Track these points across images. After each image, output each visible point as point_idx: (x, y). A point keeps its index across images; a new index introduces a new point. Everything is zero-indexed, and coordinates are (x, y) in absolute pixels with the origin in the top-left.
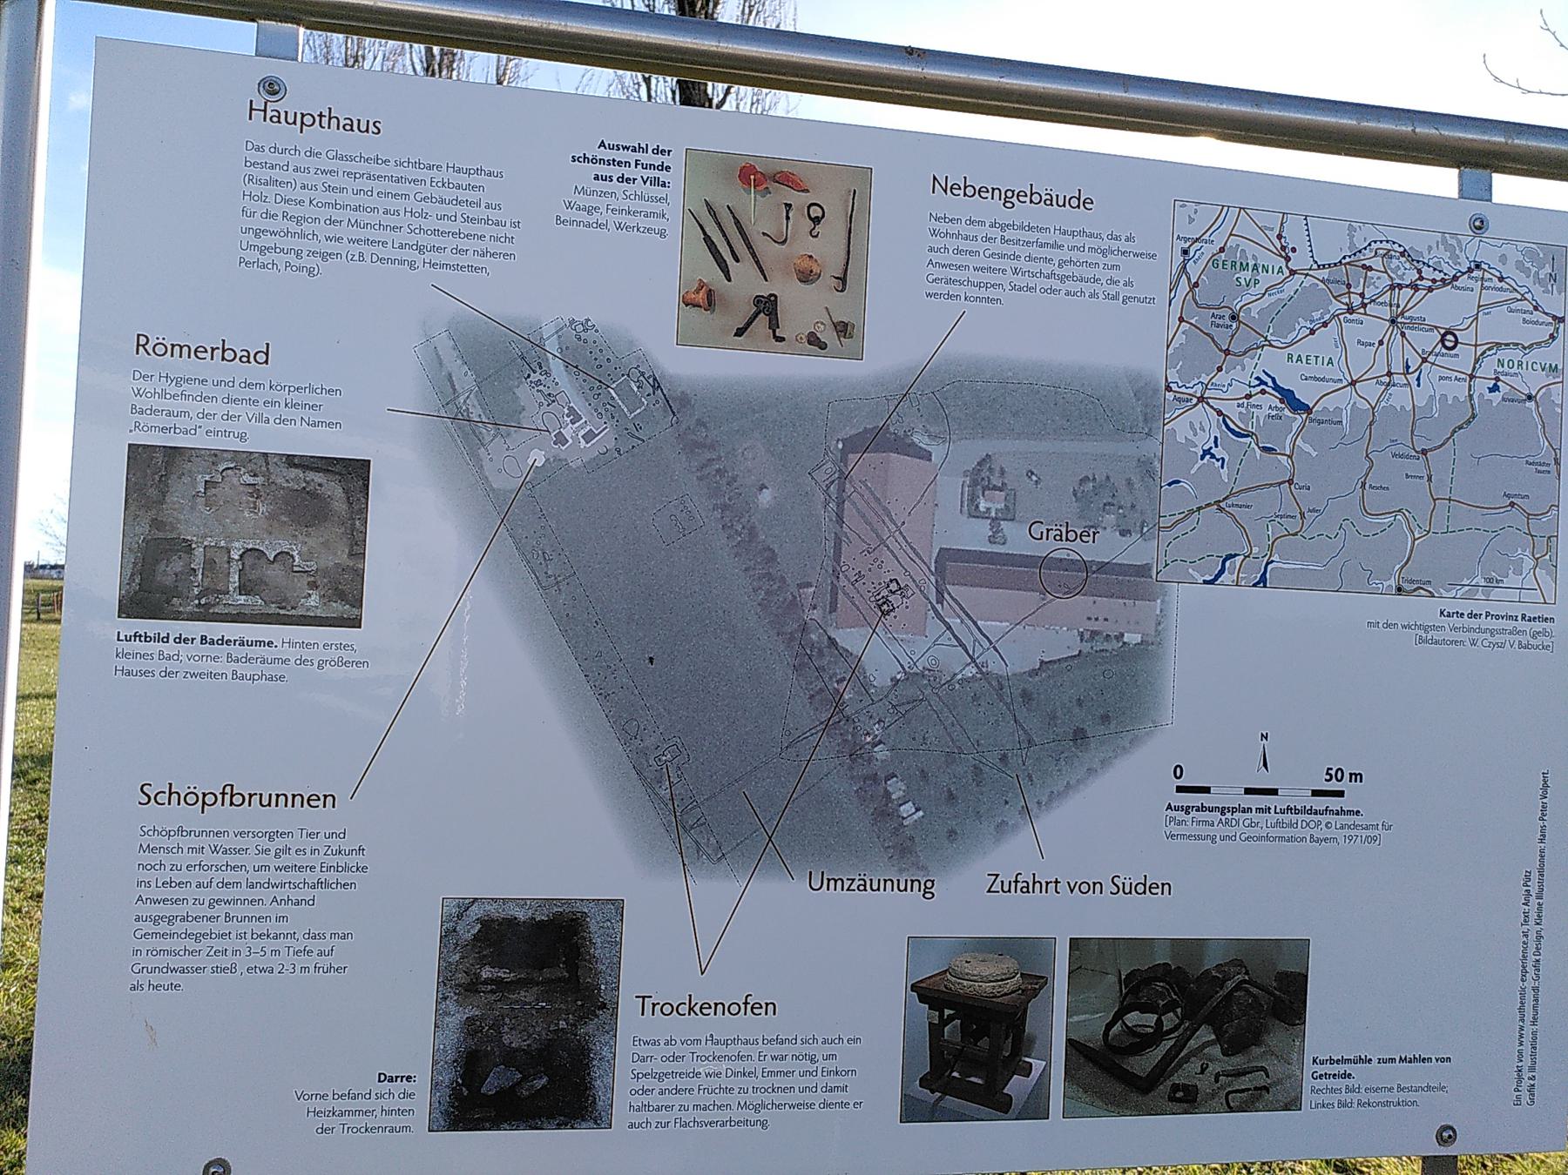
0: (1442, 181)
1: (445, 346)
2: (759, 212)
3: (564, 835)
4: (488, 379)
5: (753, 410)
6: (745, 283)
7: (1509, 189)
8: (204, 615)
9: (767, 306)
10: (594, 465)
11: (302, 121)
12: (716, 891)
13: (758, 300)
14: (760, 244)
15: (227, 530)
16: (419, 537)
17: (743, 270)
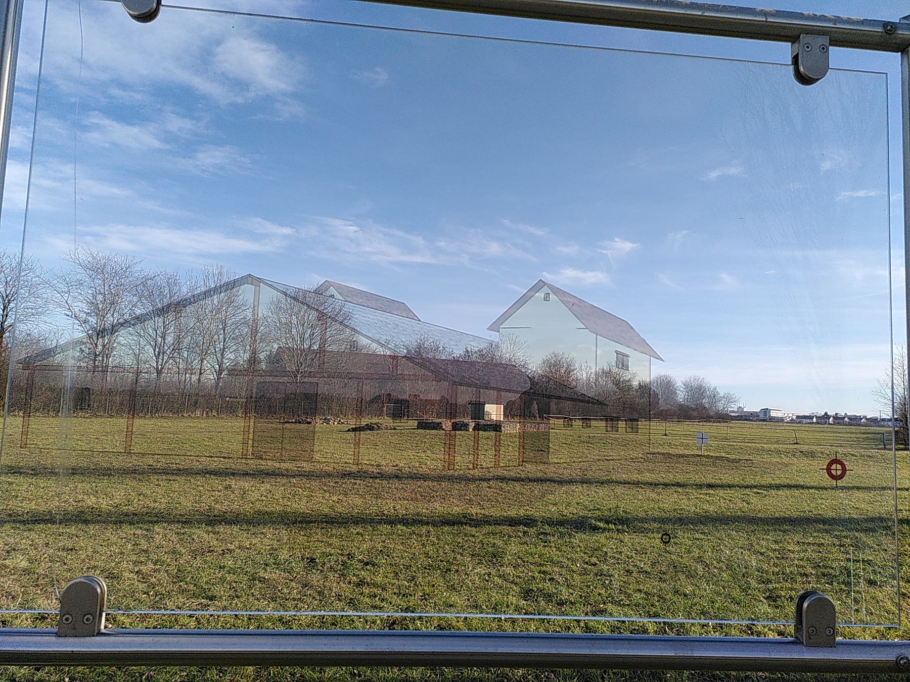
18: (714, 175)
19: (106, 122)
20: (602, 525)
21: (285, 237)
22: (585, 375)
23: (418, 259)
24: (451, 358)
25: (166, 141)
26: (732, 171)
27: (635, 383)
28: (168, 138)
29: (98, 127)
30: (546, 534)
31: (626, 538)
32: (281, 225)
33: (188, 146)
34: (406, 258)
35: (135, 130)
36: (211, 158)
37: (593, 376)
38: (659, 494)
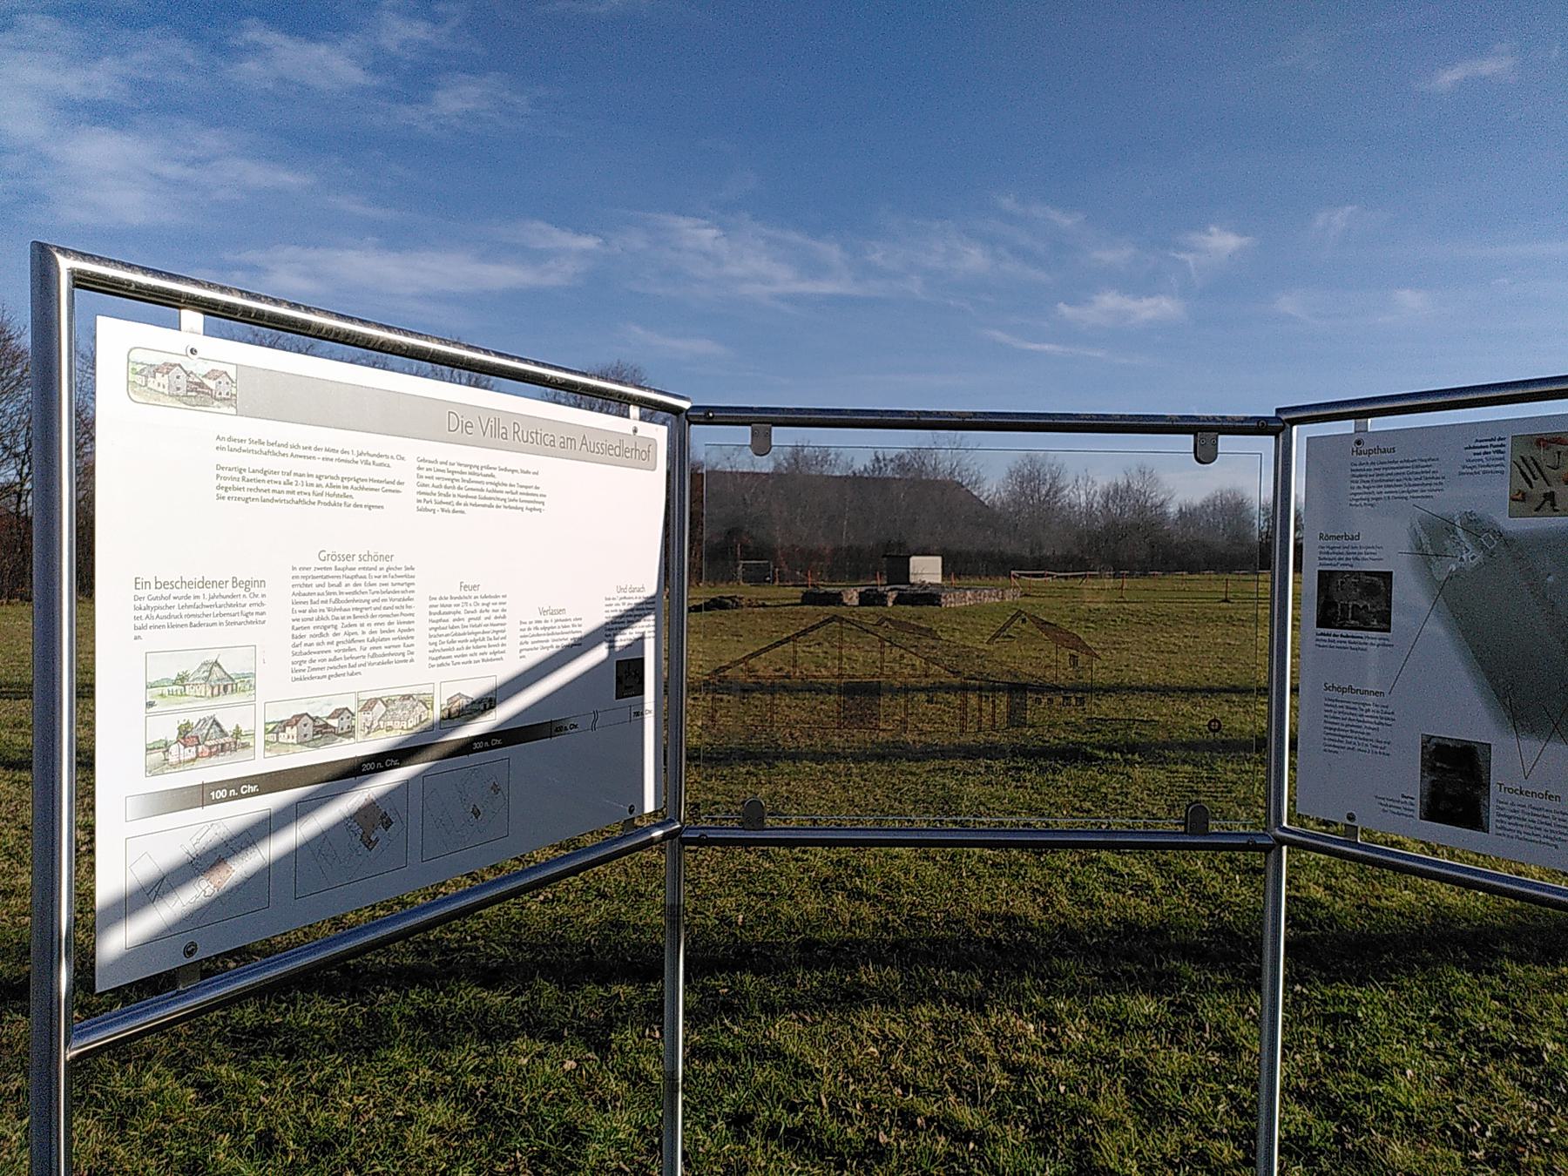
0: (1348, 427)
1: (1418, 527)
2: (1541, 454)
3: (1468, 716)
4: (1434, 538)
5: (1544, 542)
6: (1540, 487)
7: (1374, 424)
8: (1341, 627)
9: (1550, 497)
10: (1479, 567)
11: (1369, 452)
12: (1532, 745)
13: (1545, 495)
14: (1547, 472)
15: (1352, 599)
16: (1409, 594)
17: (1539, 483)
18: (1448, 78)
19: (273, 38)
20: (1102, 754)
21: (585, 253)
22: (1083, 498)
23: (827, 287)
24: (850, 473)
25: (374, 69)
26: (1487, 67)
27: (1172, 509)
28: (379, 63)
29: (256, 49)
30: (1019, 769)
31: (1137, 772)
32: (579, 231)
33: (416, 78)
34: (808, 287)
35: (320, 51)
36: (457, 100)
37: (1098, 498)
38: (1195, 705)
